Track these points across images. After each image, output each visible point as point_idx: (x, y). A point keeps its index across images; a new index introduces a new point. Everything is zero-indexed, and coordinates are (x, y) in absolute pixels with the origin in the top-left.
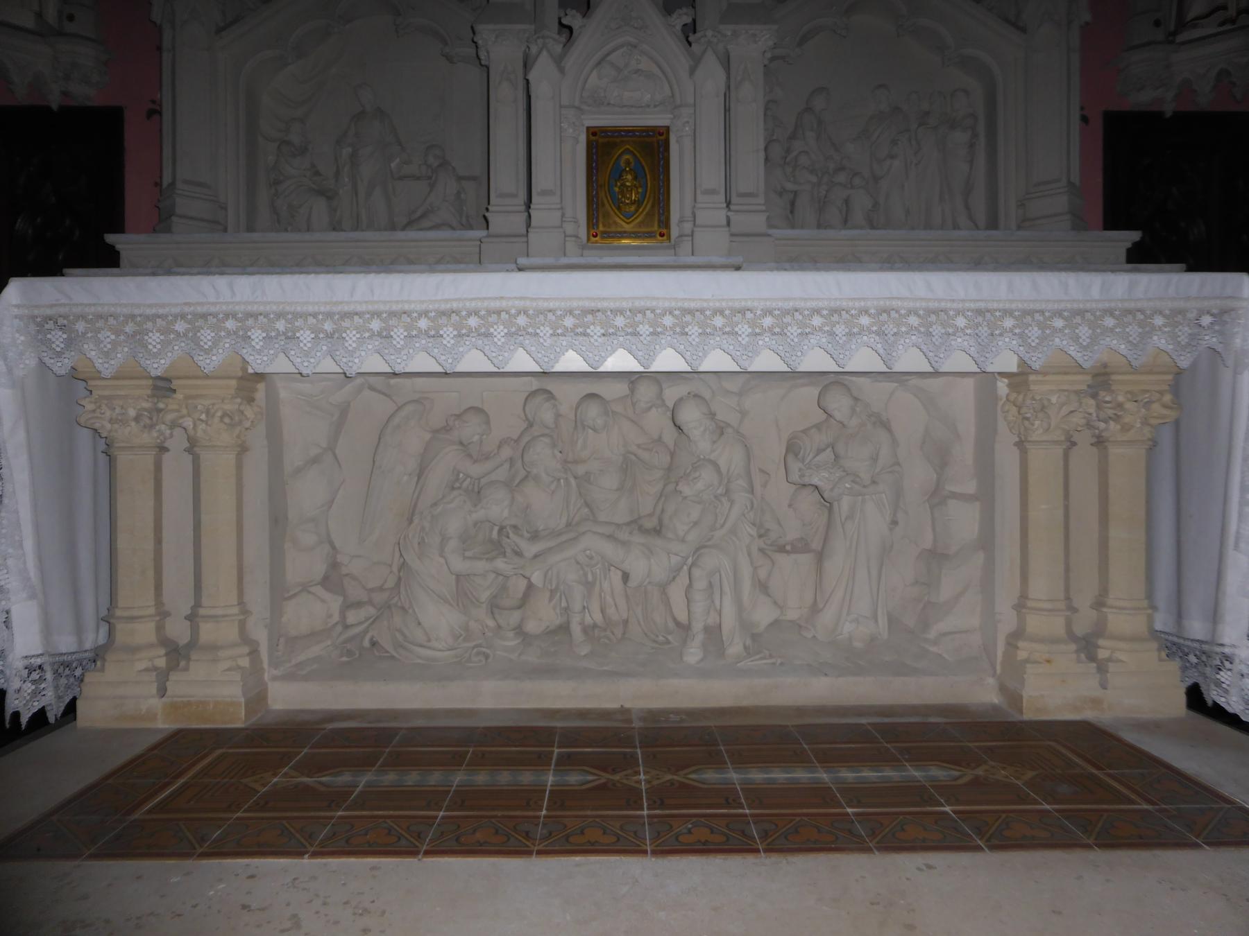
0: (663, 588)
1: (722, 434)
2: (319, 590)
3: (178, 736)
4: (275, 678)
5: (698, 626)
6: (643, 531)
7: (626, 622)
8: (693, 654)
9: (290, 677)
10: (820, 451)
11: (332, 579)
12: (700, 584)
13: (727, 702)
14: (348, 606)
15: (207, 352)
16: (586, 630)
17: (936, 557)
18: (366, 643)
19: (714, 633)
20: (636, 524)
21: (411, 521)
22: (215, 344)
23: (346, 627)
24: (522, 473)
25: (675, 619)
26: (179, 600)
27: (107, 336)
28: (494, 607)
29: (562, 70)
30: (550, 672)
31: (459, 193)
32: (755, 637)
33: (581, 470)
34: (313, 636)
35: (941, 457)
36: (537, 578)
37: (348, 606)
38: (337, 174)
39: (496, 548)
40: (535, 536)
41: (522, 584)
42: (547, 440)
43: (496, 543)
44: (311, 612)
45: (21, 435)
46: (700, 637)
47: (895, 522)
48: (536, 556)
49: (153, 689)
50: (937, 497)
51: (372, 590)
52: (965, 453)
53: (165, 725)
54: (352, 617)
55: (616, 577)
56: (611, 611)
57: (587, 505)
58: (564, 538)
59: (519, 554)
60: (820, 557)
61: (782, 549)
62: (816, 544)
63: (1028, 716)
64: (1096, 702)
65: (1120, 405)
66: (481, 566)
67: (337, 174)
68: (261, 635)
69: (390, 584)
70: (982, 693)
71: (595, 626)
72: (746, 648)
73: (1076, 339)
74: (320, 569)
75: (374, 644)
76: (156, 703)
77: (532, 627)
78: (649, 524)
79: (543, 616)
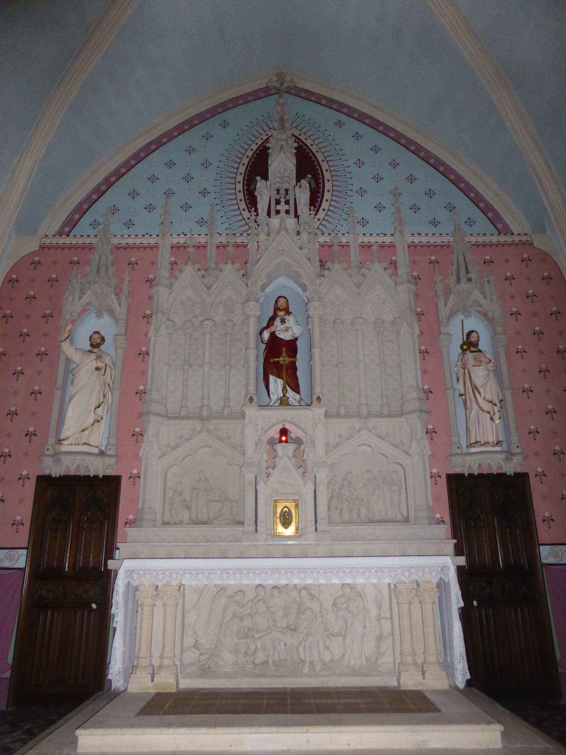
0: (297, 648)
1: (313, 599)
2: (193, 649)
3: (158, 694)
4: (181, 678)
5: (307, 661)
6: (290, 630)
7: (286, 660)
8: (306, 670)
9: (185, 677)
10: (343, 604)
11: (196, 646)
12: (308, 647)
13: (315, 685)
14: (201, 654)
15: (174, 580)
16: (274, 662)
17: (380, 638)
18: (206, 667)
19: (312, 663)
20: (288, 627)
21: (221, 627)
22: (177, 577)
23: (200, 661)
24: (254, 611)
25: (301, 659)
26: (156, 652)
27: (148, 576)
28: (246, 654)
29: (267, 486)
30: (263, 676)
31: (231, 508)
32: (325, 665)
33: (272, 609)
34: (191, 665)
35: (379, 606)
36: (259, 645)
37: (201, 654)
38: (191, 500)
39: (246, 636)
40: (258, 632)
41: (254, 647)
42: (262, 601)
43: (247, 634)
44: (190, 656)
45: (123, 603)
46: (308, 664)
47: (365, 627)
48: (258, 638)
49: (150, 679)
50: (379, 619)
51: (207, 649)
52: (386, 604)
53: (153, 691)
54: (202, 658)
55: (282, 644)
56: (281, 656)
57: (274, 621)
58: (267, 632)
59: (253, 637)
60: (344, 637)
61: (333, 635)
62: (343, 633)
63: (401, 689)
64: (421, 684)
65: (422, 592)
66: (243, 641)
67: (191, 500)
68: (178, 663)
69: (213, 646)
70: (392, 683)
71: (276, 661)
72: (322, 668)
73: (404, 575)
74: (193, 642)
75: (209, 667)
76: (151, 684)
77: (257, 661)
78: (292, 627)
79: (261, 657)
